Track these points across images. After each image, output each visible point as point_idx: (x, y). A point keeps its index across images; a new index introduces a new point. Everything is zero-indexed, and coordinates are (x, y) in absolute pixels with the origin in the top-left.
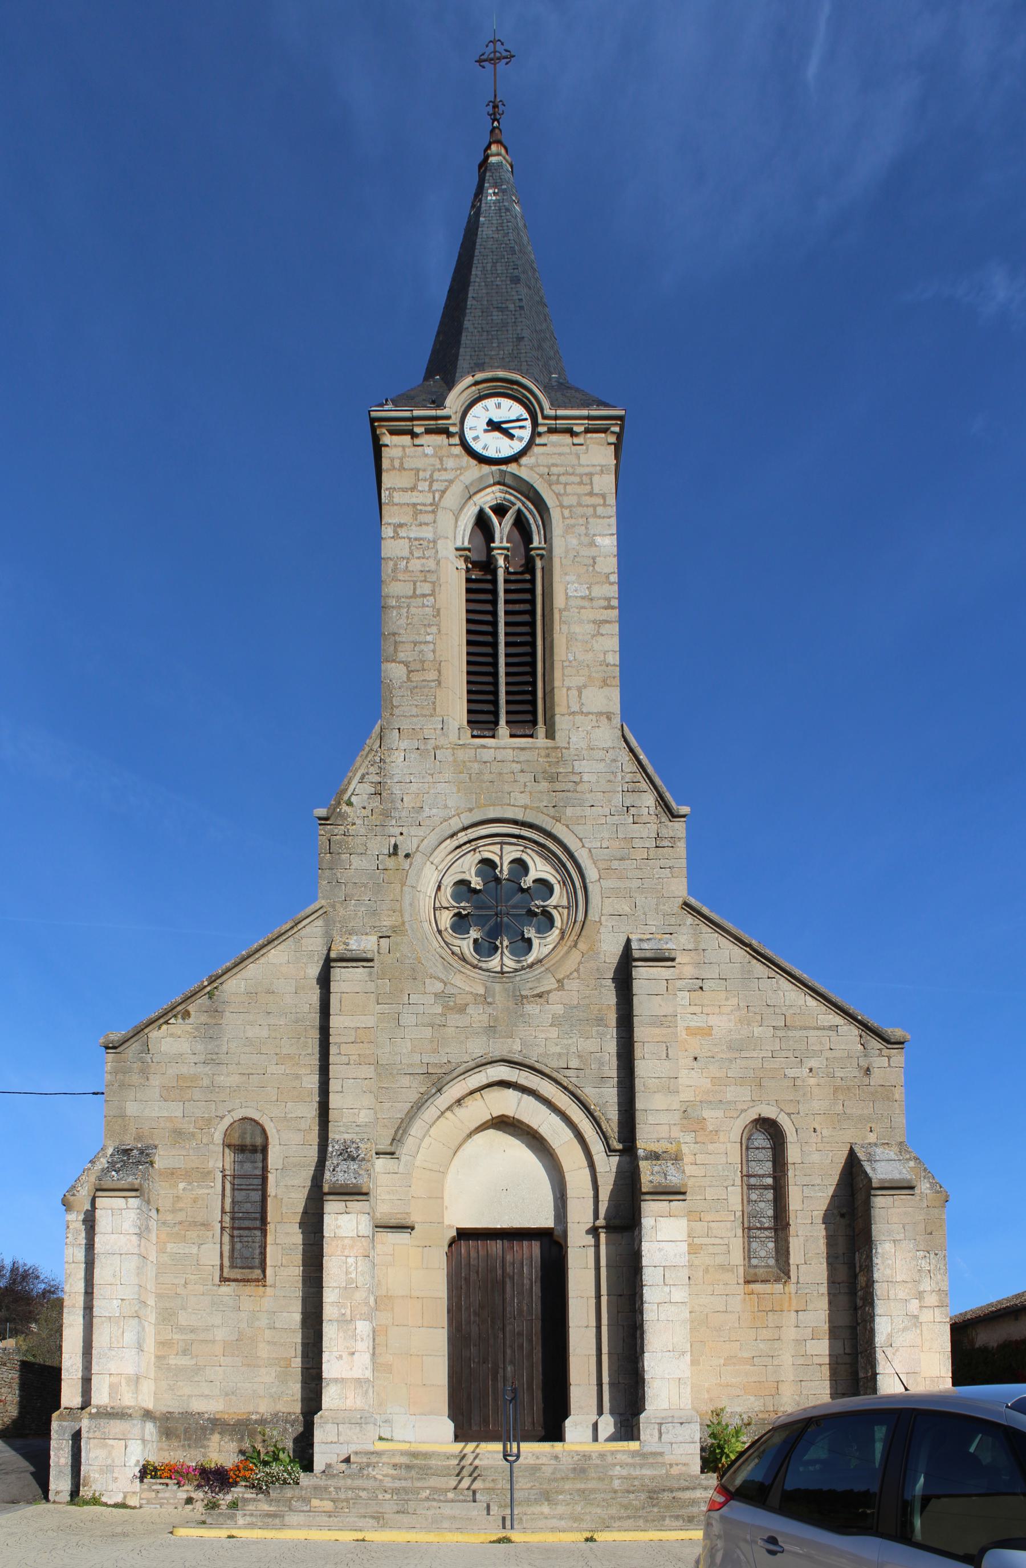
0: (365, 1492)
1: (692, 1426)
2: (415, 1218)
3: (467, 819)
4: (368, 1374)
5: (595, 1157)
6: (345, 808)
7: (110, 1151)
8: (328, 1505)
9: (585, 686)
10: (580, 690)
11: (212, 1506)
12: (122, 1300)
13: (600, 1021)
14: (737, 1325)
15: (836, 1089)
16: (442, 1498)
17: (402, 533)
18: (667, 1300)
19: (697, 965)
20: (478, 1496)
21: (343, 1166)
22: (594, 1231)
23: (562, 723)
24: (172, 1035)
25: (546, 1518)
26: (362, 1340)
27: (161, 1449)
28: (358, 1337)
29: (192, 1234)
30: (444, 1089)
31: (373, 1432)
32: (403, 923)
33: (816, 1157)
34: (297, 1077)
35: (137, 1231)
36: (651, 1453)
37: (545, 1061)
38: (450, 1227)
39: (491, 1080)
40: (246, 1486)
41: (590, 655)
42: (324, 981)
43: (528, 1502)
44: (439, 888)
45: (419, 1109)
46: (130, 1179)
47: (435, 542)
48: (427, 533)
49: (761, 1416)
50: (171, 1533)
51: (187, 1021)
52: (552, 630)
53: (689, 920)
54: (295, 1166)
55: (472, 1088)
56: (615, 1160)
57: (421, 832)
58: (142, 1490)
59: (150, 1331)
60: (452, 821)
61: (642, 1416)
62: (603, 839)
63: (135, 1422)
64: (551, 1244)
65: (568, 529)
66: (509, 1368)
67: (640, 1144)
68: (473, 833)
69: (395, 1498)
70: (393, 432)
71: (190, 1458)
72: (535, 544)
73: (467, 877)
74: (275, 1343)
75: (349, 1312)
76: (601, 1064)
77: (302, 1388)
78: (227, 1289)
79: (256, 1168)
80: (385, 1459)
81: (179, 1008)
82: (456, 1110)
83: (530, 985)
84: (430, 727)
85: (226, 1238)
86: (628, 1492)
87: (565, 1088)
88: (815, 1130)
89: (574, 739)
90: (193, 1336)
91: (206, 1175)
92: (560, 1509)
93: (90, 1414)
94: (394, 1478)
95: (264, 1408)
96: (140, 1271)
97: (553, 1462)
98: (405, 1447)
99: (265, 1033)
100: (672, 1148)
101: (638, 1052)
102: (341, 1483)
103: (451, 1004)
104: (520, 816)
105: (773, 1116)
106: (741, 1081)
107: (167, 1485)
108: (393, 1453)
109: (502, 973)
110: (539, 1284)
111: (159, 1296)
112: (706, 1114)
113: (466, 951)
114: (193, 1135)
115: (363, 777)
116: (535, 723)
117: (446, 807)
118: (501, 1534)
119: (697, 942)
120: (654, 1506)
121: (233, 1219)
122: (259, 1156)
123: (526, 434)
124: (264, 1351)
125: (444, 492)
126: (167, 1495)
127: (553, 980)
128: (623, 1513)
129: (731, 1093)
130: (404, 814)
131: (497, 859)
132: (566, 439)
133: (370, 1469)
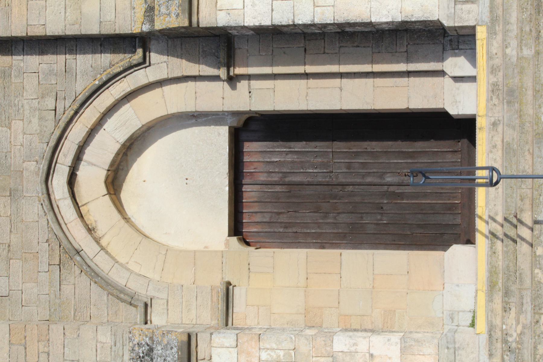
2: (217, 281)
4: (395, 338)
5: (152, 79)
26: (355, 344)
28: (353, 349)
30: (77, 247)
31: (465, 335)
36: (491, 12)
38: (227, 244)
39: (67, 194)
45: (97, 275)
56: (154, 57)
61: (447, 23)
64: (249, 129)
76: (51, 72)
80: (498, 321)
82: (99, 233)
87: (76, 113)
94: (520, 311)
97: (500, 128)
108: (490, 312)
110: (292, 144)
133: (510, 339)
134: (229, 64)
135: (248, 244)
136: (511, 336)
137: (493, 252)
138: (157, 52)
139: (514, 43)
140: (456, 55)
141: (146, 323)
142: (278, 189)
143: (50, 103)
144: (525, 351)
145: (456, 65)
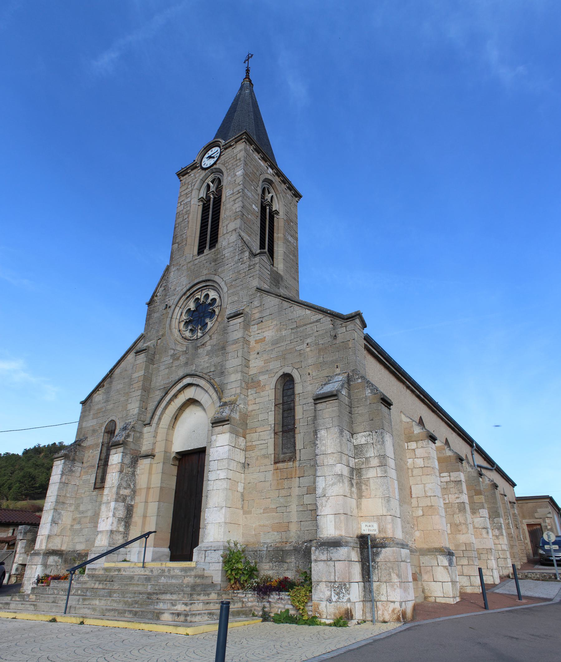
14: (269, 489)
15: (320, 350)
19: (260, 312)
38: (173, 452)
49: (278, 545)
65: (228, 175)
104: (188, 287)
114: (97, 430)
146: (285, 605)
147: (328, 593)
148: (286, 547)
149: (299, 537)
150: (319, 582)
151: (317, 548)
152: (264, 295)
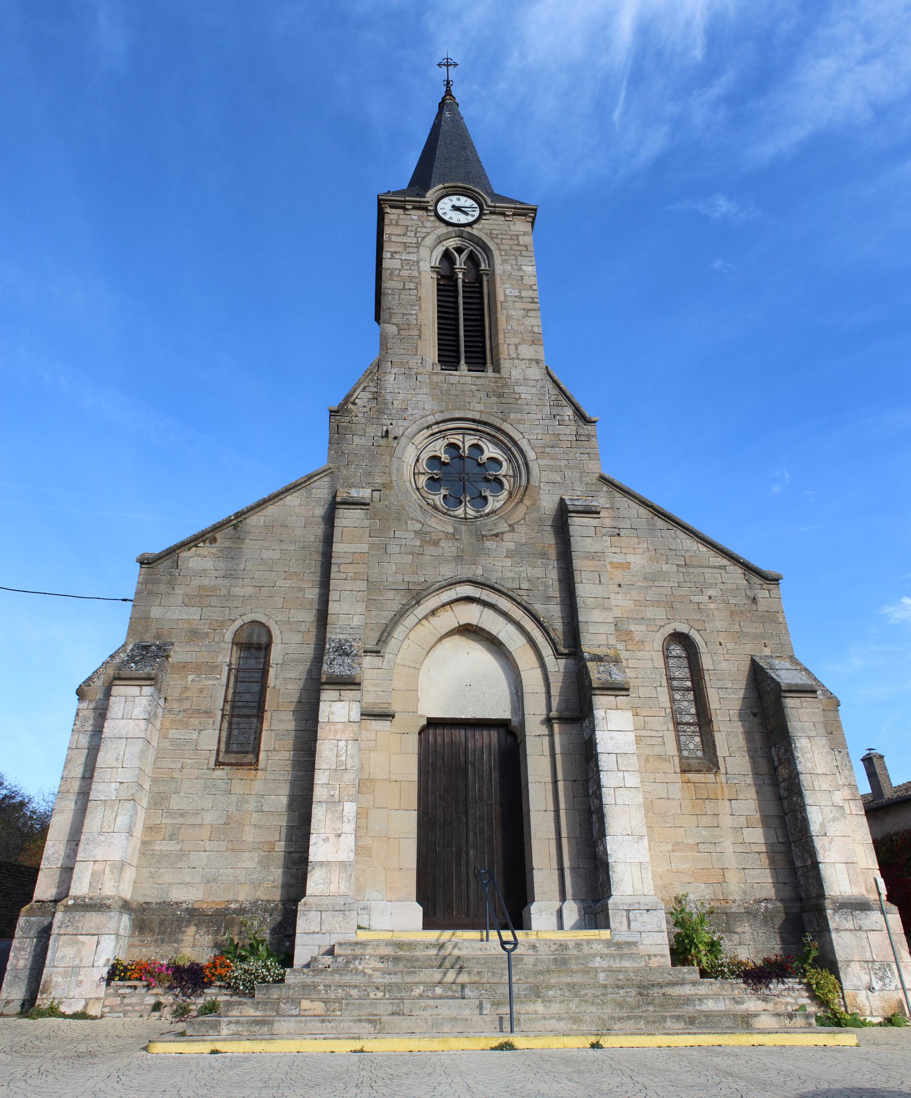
0: (356, 990)
1: (658, 913)
2: (396, 708)
3: (439, 417)
4: (352, 856)
5: (546, 659)
6: (350, 406)
7: (130, 647)
8: (319, 1007)
9: (520, 344)
10: (516, 346)
11: (181, 1013)
12: (121, 783)
13: (544, 555)
14: (679, 812)
16: (429, 994)
17: (397, 256)
18: (622, 785)
20: (467, 992)
21: (339, 660)
22: (549, 721)
23: (505, 364)
24: (199, 555)
25: (545, 1018)
26: (349, 820)
27: (131, 945)
28: (345, 819)
29: (195, 721)
30: (422, 602)
31: (355, 919)
32: (391, 482)
33: (725, 665)
34: (301, 589)
35: (147, 716)
36: (626, 943)
37: (502, 583)
38: (422, 716)
39: (459, 596)
40: (220, 987)
41: (522, 327)
42: (330, 520)
43: (527, 999)
44: (418, 460)
45: (401, 616)
46: (148, 669)
47: (418, 262)
48: (413, 257)
50: (146, 1049)
51: (213, 545)
52: (496, 312)
53: (605, 488)
54: (293, 661)
55: (444, 601)
56: (562, 662)
57: (406, 423)
58: (107, 995)
59: (141, 814)
60: (429, 418)
61: (610, 901)
62: (538, 434)
63: (112, 914)
64: (509, 734)
66: (471, 852)
67: (584, 648)
68: (443, 427)
69: (387, 996)
70: (392, 207)
71: (159, 954)
72: (483, 267)
73: (438, 454)
74: (260, 827)
75: (337, 793)
76: (547, 587)
77: (284, 873)
78: (219, 773)
79: (259, 663)
80: (369, 951)
81: (209, 535)
82: (431, 619)
83: (488, 528)
84: (413, 362)
85: (225, 725)
86: (618, 987)
87: (519, 604)
88: (720, 644)
89: (513, 373)
90: (181, 820)
91: (214, 668)
92: (555, 1008)
93: (66, 906)
94: (384, 972)
95: (244, 895)
96: (142, 754)
97: (531, 952)
98: (387, 936)
99: (277, 556)
100: (611, 652)
101: (577, 578)
102: (329, 979)
103: (427, 538)
104: (477, 417)
105: (686, 631)
106: (657, 604)
107: (135, 987)
108: (378, 944)
109: (466, 519)
110: (497, 771)
111: (154, 780)
112: (633, 627)
113: (438, 503)
114: (207, 634)
115: (365, 388)
116: (485, 364)
117: (424, 409)
118: (502, 1040)
119: (612, 503)
120: (649, 1004)
121: (233, 707)
122: (263, 653)
123: (477, 214)
124: (250, 835)
125: (424, 238)
126: (134, 1000)
127: (506, 525)
128: (618, 1013)
129: (650, 612)
130: (393, 412)
131: (460, 444)
132: (502, 218)
133: (357, 962)
134: (561, 719)
135: (420, 733)
136: (360, 964)
137: (428, 946)
138: (566, 664)
139: (605, 964)
140: (579, 911)
141: (365, 652)
142: (462, 758)
143: (525, 585)
144: (350, 977)
145: (571, 911)
146: (796, 998)
147: (865, 978)
148: (731, 908)
149: (745, 893)
150: (848, 962)
151: (835, 911)
152: (617, 495)
